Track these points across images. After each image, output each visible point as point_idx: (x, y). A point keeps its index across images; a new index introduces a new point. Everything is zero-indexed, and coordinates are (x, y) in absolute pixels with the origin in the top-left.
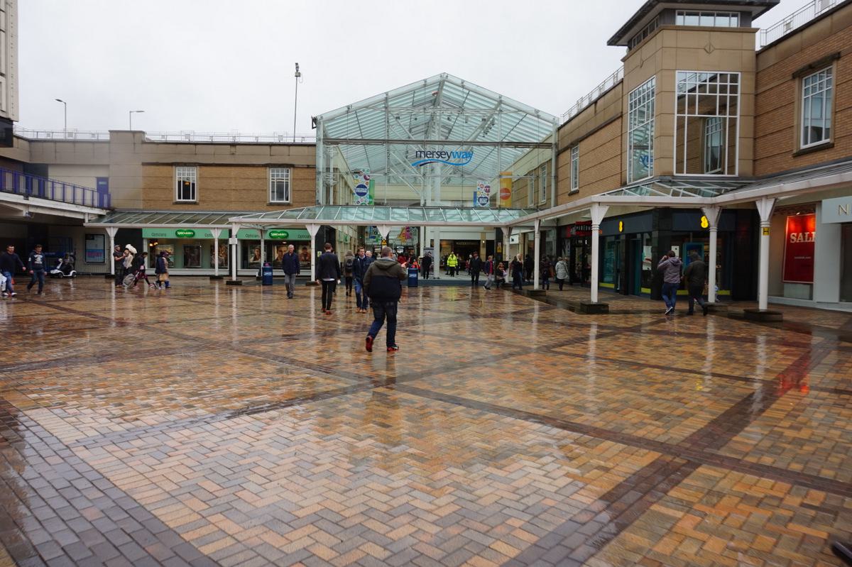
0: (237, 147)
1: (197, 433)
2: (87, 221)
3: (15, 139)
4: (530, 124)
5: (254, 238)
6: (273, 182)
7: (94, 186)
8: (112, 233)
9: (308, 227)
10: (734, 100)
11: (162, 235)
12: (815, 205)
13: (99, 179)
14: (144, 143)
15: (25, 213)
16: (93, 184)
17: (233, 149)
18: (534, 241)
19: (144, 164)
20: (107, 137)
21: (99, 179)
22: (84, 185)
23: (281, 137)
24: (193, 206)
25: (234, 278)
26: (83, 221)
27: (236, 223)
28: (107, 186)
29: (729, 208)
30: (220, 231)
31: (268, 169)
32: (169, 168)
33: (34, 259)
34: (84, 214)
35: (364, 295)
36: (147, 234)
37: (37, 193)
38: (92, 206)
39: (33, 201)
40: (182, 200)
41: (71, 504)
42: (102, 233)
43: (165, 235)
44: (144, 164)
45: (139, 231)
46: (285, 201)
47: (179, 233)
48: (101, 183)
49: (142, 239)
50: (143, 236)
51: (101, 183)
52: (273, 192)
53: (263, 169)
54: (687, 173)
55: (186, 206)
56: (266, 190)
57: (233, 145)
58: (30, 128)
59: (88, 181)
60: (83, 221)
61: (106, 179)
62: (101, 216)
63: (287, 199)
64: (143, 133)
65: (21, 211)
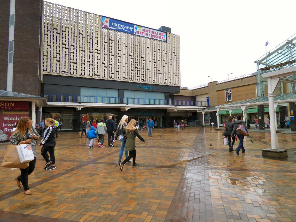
0: (244, 79)
1: (232, 197)
4: (271, 58)
5: (237, 113)
6: (226, 94)
8: (203, 114)
9: (229, 111)
10: (230, 93)
11: (238, 112)
14: (217, 84)
16: (205, 100)
18: (243, 114)
23: (222, 81)
25: (218, 128)
29: (149, 108)
30: (231, 111)
31: (255, 85)
34: (197, 108)
35: (44, 132)
37: (192, 105)
39: (178, 107)
40: (228, 101)
41: (193, 211)
42: (201, 113)
43: (223, 113)
47: (227, 112)
52: (231, 97)
53: (253, 85)
56: (254, 93)
57: (242, 79)
60: (197, 110)
63: (231, 100)
64: (216, 81)
65: (174, 110)
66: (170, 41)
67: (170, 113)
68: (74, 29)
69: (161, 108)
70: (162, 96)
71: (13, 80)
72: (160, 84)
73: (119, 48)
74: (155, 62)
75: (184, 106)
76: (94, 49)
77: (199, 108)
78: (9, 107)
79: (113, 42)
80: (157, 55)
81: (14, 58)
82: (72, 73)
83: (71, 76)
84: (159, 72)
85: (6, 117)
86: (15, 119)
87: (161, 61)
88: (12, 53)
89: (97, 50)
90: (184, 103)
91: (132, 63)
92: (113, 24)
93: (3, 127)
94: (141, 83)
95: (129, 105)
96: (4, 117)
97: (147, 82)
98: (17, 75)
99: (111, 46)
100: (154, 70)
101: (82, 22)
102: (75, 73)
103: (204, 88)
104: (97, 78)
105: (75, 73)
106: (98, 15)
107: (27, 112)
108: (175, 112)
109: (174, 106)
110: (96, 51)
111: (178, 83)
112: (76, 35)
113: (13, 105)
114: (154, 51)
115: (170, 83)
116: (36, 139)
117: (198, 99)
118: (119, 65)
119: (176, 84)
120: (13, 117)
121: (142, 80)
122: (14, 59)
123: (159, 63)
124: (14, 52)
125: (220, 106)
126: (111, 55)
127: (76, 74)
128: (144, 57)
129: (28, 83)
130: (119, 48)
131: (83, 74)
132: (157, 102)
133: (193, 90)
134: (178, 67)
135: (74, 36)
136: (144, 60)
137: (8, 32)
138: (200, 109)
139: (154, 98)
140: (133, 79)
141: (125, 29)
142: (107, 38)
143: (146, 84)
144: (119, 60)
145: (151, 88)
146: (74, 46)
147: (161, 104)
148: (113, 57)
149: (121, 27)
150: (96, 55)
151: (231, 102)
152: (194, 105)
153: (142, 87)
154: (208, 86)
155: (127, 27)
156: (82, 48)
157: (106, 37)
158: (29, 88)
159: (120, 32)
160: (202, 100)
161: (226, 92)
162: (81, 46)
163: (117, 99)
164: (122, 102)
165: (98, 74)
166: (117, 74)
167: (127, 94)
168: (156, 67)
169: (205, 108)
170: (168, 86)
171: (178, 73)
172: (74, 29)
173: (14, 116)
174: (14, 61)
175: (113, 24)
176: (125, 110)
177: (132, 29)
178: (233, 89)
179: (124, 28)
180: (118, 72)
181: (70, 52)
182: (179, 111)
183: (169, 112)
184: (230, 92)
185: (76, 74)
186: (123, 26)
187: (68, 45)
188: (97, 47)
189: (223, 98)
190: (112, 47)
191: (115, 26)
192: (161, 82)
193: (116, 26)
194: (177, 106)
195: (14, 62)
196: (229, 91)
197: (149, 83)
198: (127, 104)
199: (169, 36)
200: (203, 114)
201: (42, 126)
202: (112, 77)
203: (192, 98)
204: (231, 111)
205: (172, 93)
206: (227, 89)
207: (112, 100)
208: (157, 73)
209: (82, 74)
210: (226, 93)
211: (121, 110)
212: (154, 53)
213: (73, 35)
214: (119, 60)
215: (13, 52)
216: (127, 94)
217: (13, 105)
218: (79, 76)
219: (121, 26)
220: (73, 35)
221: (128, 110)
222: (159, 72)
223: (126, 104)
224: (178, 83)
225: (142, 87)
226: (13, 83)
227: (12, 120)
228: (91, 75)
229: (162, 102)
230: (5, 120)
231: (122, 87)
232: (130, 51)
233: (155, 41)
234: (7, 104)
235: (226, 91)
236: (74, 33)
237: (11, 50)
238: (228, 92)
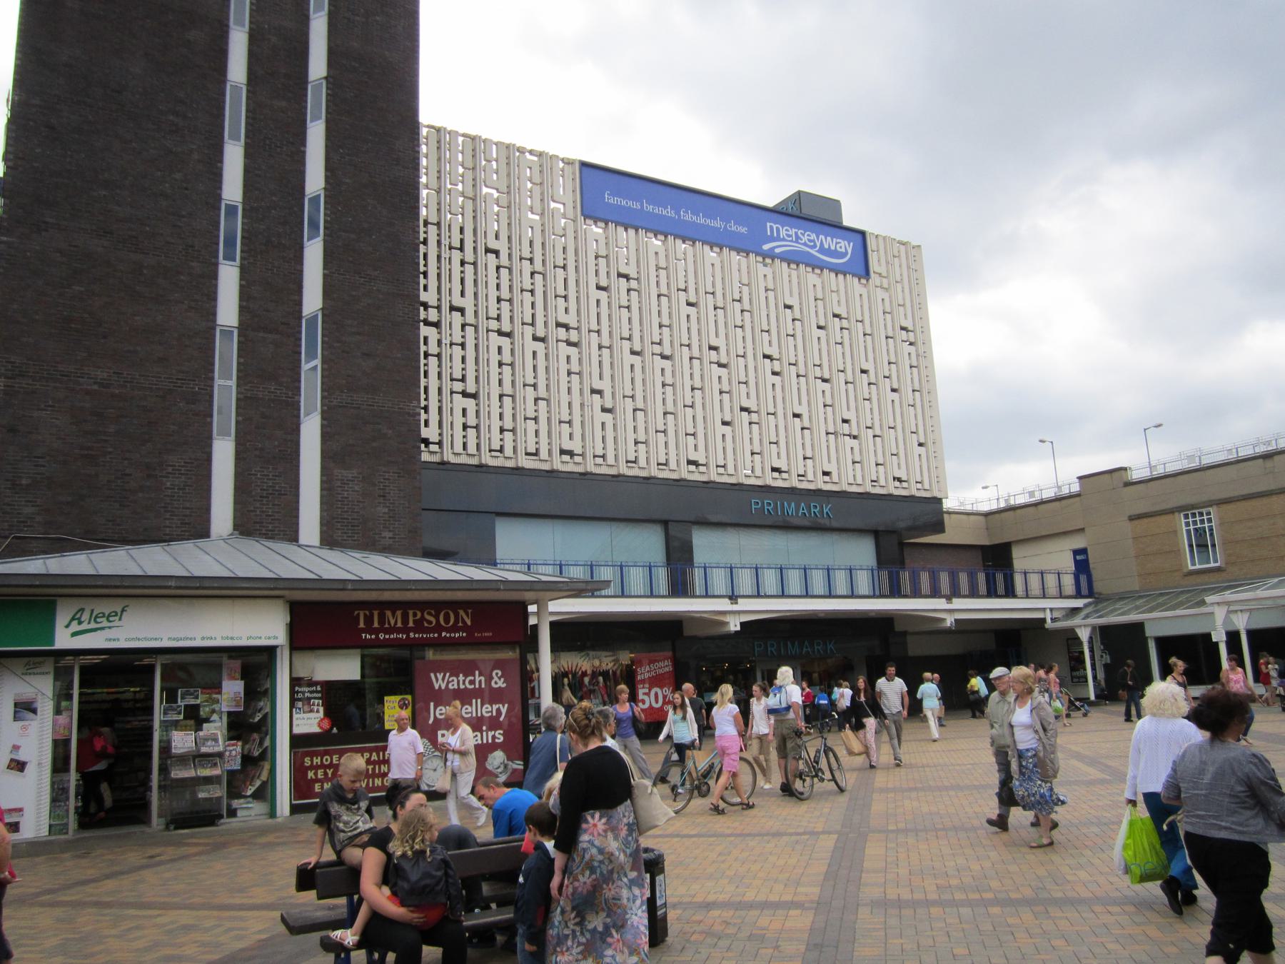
2: (1049, 620)
3: (946, 516)
6: (1188, 532)
7: (1071, 566)
10: (1211, 529)
12: (218, 667)
13: (1076, 552)
14: (1128, 484)
15: (949, 621)
16: (1068, 563)
17: (1269, 464)
19: (1131, 518)
20: (1076, 488)
21: (1076, 552)
22: (1038, 567)
24: (1216, 576)
26: (1044, 620)
27: (1218, 603)
28: (1086, 561)
30: (1246, 616)
32: (1169, 517)
33: (359, 775)
34: (1044, 609)
36: (1151, 631)
37: (967, 593)
38: (1061, 596)
39: (958, 603)
40: (1198, 567)
44: (1131, 518)
45: (1138, 627)
46: (1212, 565)
48: (1078, 558)
49: (1145, 639)
50: (1148, 634)
51: (1078, 558)
54: (329, 540)
55: (1205, 578)
57: (1267, 456)
58: (1019, 490)
59: (1059, 557)
60: (1044, 620)
61: (1083, 551)
62: (1075, 611)
63: (1216, 561)
64: (1125, 469)
66: (883, 270)
67: (909, 639)
68: (462, 230)
69: (822, 615)
70: (862, 552)
71: (322, 496)
72: (854, 489)
73: (498, 285)
74: (724, 361)
75: (906, 596)
76: (552, 324)
77: (1051, 610)
78: (455, 629)
79: (634, 284)
80: (615, 306)
81: (323, 390)
82: (458, 447)
83: (453, 459)
84: (845, 430)
85: (440, 676)
86: (472, 682)
87: (801, 363)
88: (307, 362)
89: (567, 327)
90: (944, 579)
91: (667, 382)
92: (771, 228)
93: (431, 721)
94: (769, 487)
95: (743, 604)
96: (432, 675)
97: (795, 483)
98: (339, 472)
99: (530, 287)
100: (822, 421)
101: (496, 195)
102: (472, 448)
103: (1057, 504)
104: (570, 468)
105: (472, 448)
106: (562, 160)
107: (513, 649)
108: (948, 632)
109: (940, 603)
110: (562, 333)
111: (934, 480)
112: (469, 257)
113: (469, 623)
114: (593, 287)
115: (897, 484)
116: (342, 800)
117: (1022, 559)
118: (500, 381)
119: (927, 487)
120: (466, 676)
121: (563, 452)
122: (323, 398)
123: (595, 347)
124: (323, 362)
125: (1229, 596)
126: (528, 337)
127: (475, 452)
128: (573, 324)
129: (382, 510)
130: (498, 285)
131: (508, 451)
132: (840, 582)
133: (987, 515)
134: (926, 398)
135: (463, 263)
136: (777, 369)
137: (301, 272)
138: (1056, 615)
139: (830, 563)
140: (611, 460)
141: (822, 250)
142: (608, 266)
143: (793, 491)
144: (500, 353)
145: (791, 508)
146: (462, 311)
147: (839, 592)
148: (539, 346)
149: (805, 244)
150: (564, 350)
151: (1218, 569)
152: (1010, 593)
153: (776, 507)
154: (1078, 495)
155: (822, 237)
156: (498, 318)
157: (602, 262)
158: (387, 534)
159: (603, 225)
160: (1044, 562)
161: (1187, 524)
162: (493, 313)
163: (662, 575)
164: (679, 588)
165: (576, 446)
166: (531, 434)
167: (709, 547)
168: (669, 380)
169: (1079, 603)
170: (889, 497)
171: (929, 431)
172: (462, 230)
173: (468, 668)
174: (322, 405)
175: (771, 228)
176: (725, 630)
177: (850, 251)
178: (1225, 507)
179: (815, 246)
180: (536, 419)
181: (446, 341)
182: (966, 628)
183: (904, 634)
184: (1210, 520)
185: (475, 452)
186: (813, 236)
187: (439, 308)
188: (566, 310)
189: (1178, 552)
190: (532, 291)
191: (778, 239)
192: (860, 481)
193: (784, 240)
194: (954, 600)
195: (323, 412)
196: (1201, 514)
197: (804, 485)
198: (733, 598)
199: (875, 248)
200: (1084, 635)
201: (494, 723)
202: (502, 447)
203: (993, 561)
204: (1246, 616)
205: (902, 532)
206: (1193, 507)
207: (636, 578)
208: (835, 433)
209: (501, 450)
210: (1184, 529)
211: (688, 632)
212: (595, 294)
213: (457, 256)
214: (500, 353)
215: (317, 362)
216: (709, 547)
217: (469, 623)
218: (492, 462)
219: (805, 239)
220: (457, 256)
221: (738, 628)
222: (845, 430)
223: (731, 598)
224: (934, 480)
225: (776, 507)
226: (322, 510)
227: (462, 687)
228: (544, 454)
229: (863, 582)
230: (437, 687)
231: (680, 513)
232: (457, 288)
233: (765, 265)
234: (447, 619)
235: (1186, 517)
236: (461, 249)
237: (311, 356)
238: (1195, 523)
